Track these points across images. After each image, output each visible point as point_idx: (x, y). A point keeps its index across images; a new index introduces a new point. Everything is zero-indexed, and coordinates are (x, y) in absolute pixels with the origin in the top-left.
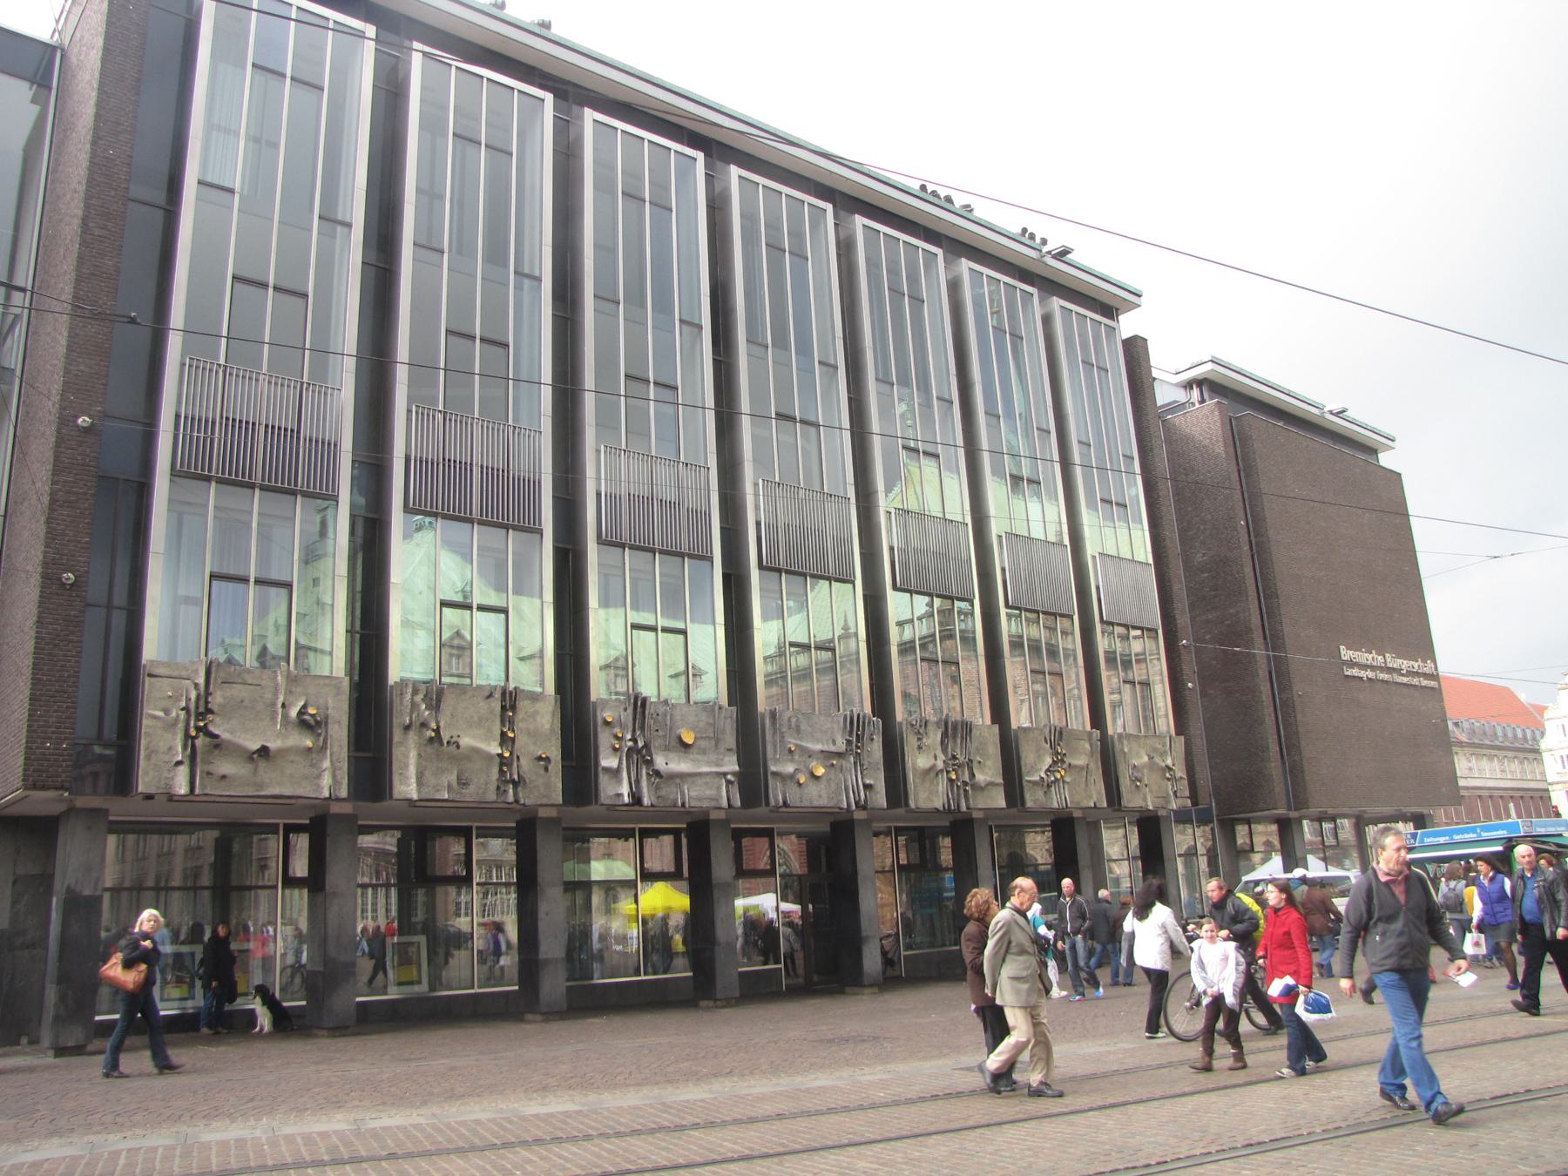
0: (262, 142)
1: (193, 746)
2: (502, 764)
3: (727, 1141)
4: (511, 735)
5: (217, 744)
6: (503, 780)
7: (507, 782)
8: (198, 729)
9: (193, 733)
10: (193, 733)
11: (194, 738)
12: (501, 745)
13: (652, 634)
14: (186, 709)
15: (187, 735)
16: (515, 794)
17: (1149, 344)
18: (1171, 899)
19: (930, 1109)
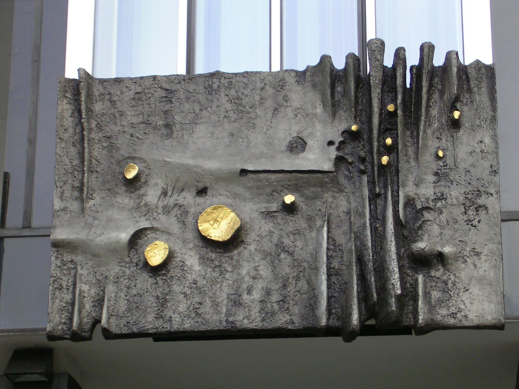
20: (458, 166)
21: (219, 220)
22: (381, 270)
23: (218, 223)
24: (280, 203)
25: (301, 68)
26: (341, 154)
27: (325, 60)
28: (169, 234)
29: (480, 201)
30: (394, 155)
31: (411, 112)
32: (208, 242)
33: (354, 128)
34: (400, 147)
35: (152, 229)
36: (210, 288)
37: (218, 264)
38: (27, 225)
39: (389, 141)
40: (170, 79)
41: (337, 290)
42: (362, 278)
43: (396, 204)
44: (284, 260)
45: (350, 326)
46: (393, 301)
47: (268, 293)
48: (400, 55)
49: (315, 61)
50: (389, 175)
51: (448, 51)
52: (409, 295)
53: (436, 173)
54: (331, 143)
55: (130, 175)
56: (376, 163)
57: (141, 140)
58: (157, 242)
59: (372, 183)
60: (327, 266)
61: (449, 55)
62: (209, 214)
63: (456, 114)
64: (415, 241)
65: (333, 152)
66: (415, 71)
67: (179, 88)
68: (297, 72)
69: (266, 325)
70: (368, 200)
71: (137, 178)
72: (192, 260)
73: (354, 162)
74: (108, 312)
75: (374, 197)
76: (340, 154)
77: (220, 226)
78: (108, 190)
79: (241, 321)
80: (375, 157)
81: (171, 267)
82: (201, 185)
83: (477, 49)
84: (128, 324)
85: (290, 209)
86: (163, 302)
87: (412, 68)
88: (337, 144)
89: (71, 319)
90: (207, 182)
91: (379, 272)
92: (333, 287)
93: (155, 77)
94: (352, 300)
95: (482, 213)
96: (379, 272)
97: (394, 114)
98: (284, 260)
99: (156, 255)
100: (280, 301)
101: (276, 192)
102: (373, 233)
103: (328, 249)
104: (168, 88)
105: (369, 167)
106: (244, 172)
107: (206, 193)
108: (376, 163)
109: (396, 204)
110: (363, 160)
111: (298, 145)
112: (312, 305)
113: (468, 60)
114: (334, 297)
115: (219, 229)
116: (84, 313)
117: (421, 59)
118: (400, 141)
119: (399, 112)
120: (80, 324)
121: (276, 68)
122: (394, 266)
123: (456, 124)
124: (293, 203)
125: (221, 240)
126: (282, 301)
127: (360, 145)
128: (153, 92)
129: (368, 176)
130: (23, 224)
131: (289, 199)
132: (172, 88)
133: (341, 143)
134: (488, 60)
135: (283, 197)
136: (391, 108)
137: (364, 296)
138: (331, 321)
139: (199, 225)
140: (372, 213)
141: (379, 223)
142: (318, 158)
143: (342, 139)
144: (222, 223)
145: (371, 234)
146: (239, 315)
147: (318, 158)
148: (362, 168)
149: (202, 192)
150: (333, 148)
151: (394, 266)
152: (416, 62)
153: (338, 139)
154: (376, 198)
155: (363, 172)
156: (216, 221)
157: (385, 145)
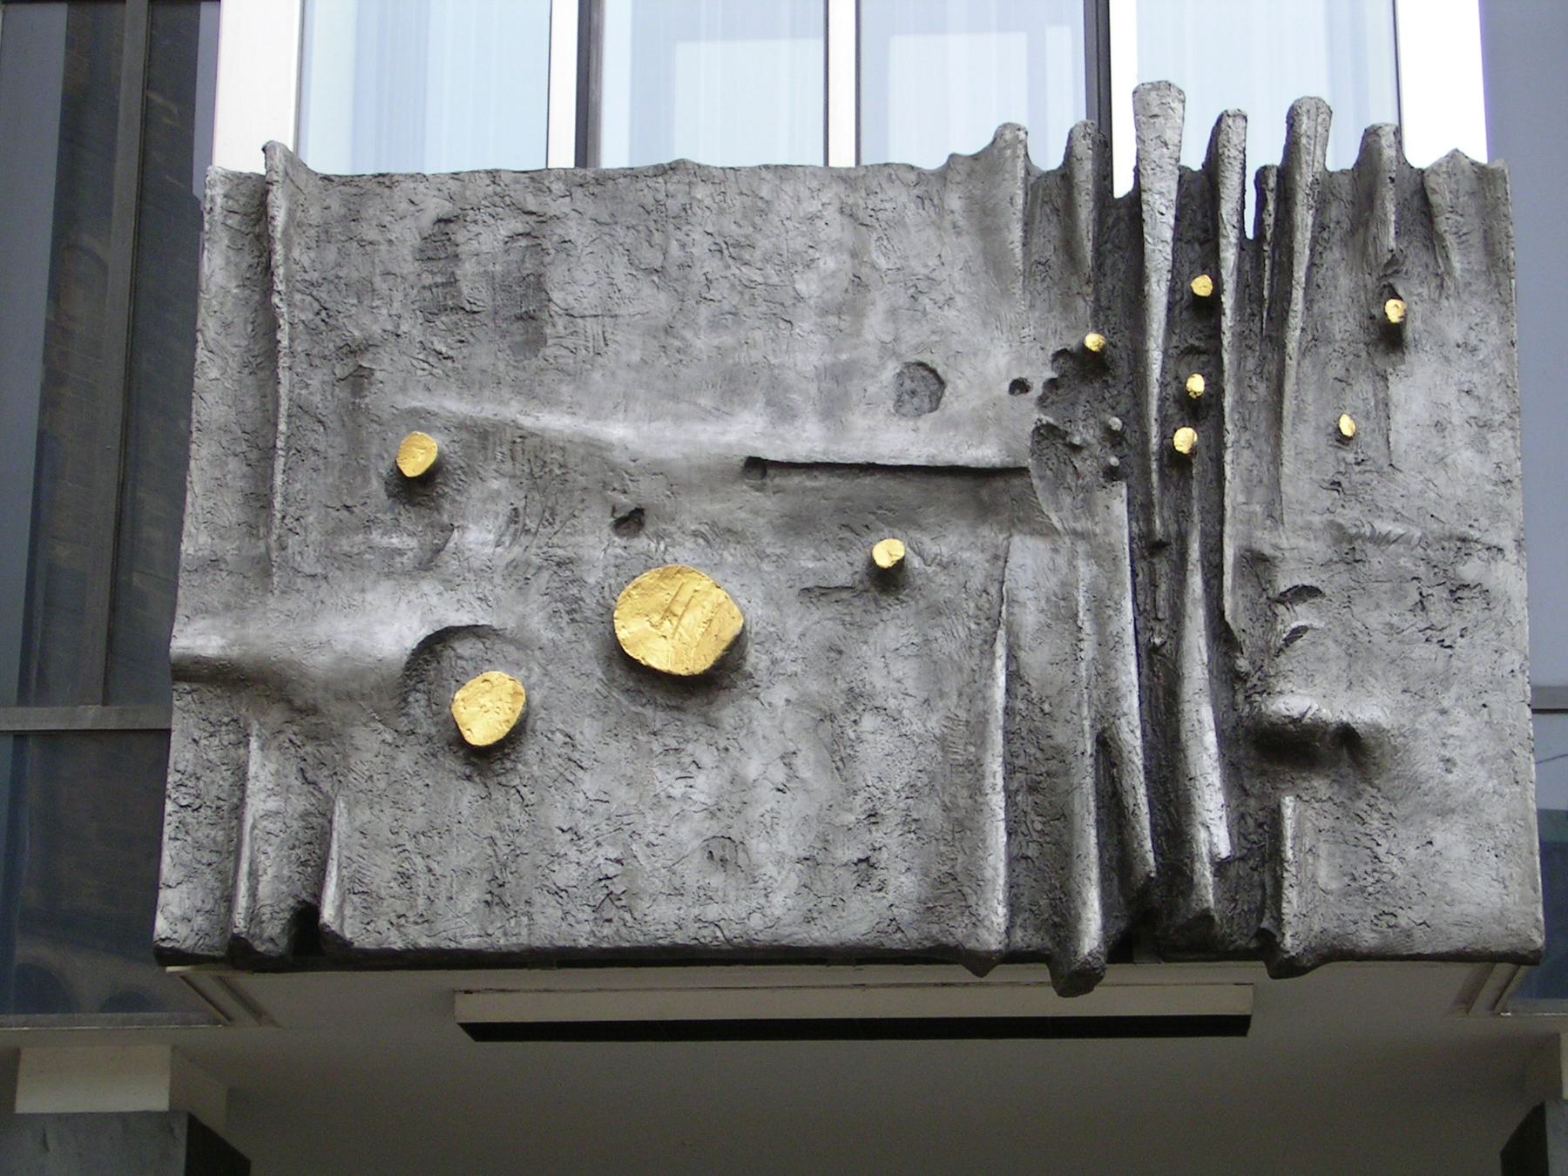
20: (1398, 465)
21: (678, 610)
23: (675, 621)
24: (860, 566)
25: (932, 161)
26: (1051, 420)
27: (1007, 142)
28: (522, 644)
29: (1469, 570)
30: (1208, 424)
31: (1261, 299)
33: (1093, 341)
34: (1228, 401)
35: (473, 631)
37: (674, 744)
39: (1196, 384)
40: (537, 179)
41: (1035, 836)
43: (1214, 573)
44: (870, 737)
45: (1076, 953)
46: (1205, 874)
49: (973, 142)
51: (1367, 125)
52: (1261, 846)
53: (1334, 483)
54: (1019, 386)
55: (415, 463)
57: (449, 363)
58: (494, 675)
59: (1141, 509)
60: (1006, 764)
61: (1371, 137)
62: (647, 592)
63: (1393, 311)
64: (1267, 691)
65: (1027, 414)
66: (1272, 182)
67: (567, 210)
68: (920, 173)
69: (817, 934)
70: (1128, 561)
71: (429, 478)
73: (1089, 445)
74: (339, 885)
75: (1148, 547)
76: (1048, 419)
77: (680, 629)
78: (347, 507)
79: (741, 922)
80: (1154, 430)
81: (530, 751)
82: (627, 502)
83: (1445, 122)
84: (403, 921)
85: (889, 581)
87: (1262, 174)
88: (1037, 389)
89: (229, 899)
90: (646, 491)
91: (1164, 784)
92: (1023, 828)
93: (493, 175)
94: (1079, 867)
95: (1473, 610)
96: (1164, 784)
97: (1209, 308)
98: (870, 737)
99: (484, 711)
100: (860, 861)
101: (858, 524)
102: (1145, 671)
103: (1009, 711)
104: (533, 209)
105: (1134, 461)
106: (757, 466)
107: (641, 525)
109: (1214, 573)
110: (1114, 439)
112: (952, 887)
113: (1422, 153)
114: (1027, 858)
115: (671, 637)
116: (264, 889)
117: (1292, 146)
118: (1229, 389)
119: (1228, 301)
120: (253, 916)
121: (842, 157)
123: (1391, 339)
124: (900, 565)
125: (684, 673)
126: (867, 860)
127: (1107, 395)
128: (486, 218)
129: (1129, 487)
131: (886, 552)
132: (546, 209)
133: (1052, 384)
134: (1478, 152)
135: (871, 545)
136: (1202, 286)
137: (1118, 860)
138: (1018, 934)
139: (618, 624)
140: (1141, 598)
141: (1160, 634)
143: (1054, 375)
144: (685, 621)
145: (1139, 666)
148: (1114, 461)
149: (631, 521)
150: (1028, 401)
152: (1275, 158)
153: (1040, 374)
154: (1152, 555)
155: (1112, 474)
156: (668, 612)
157: (1184, 394)
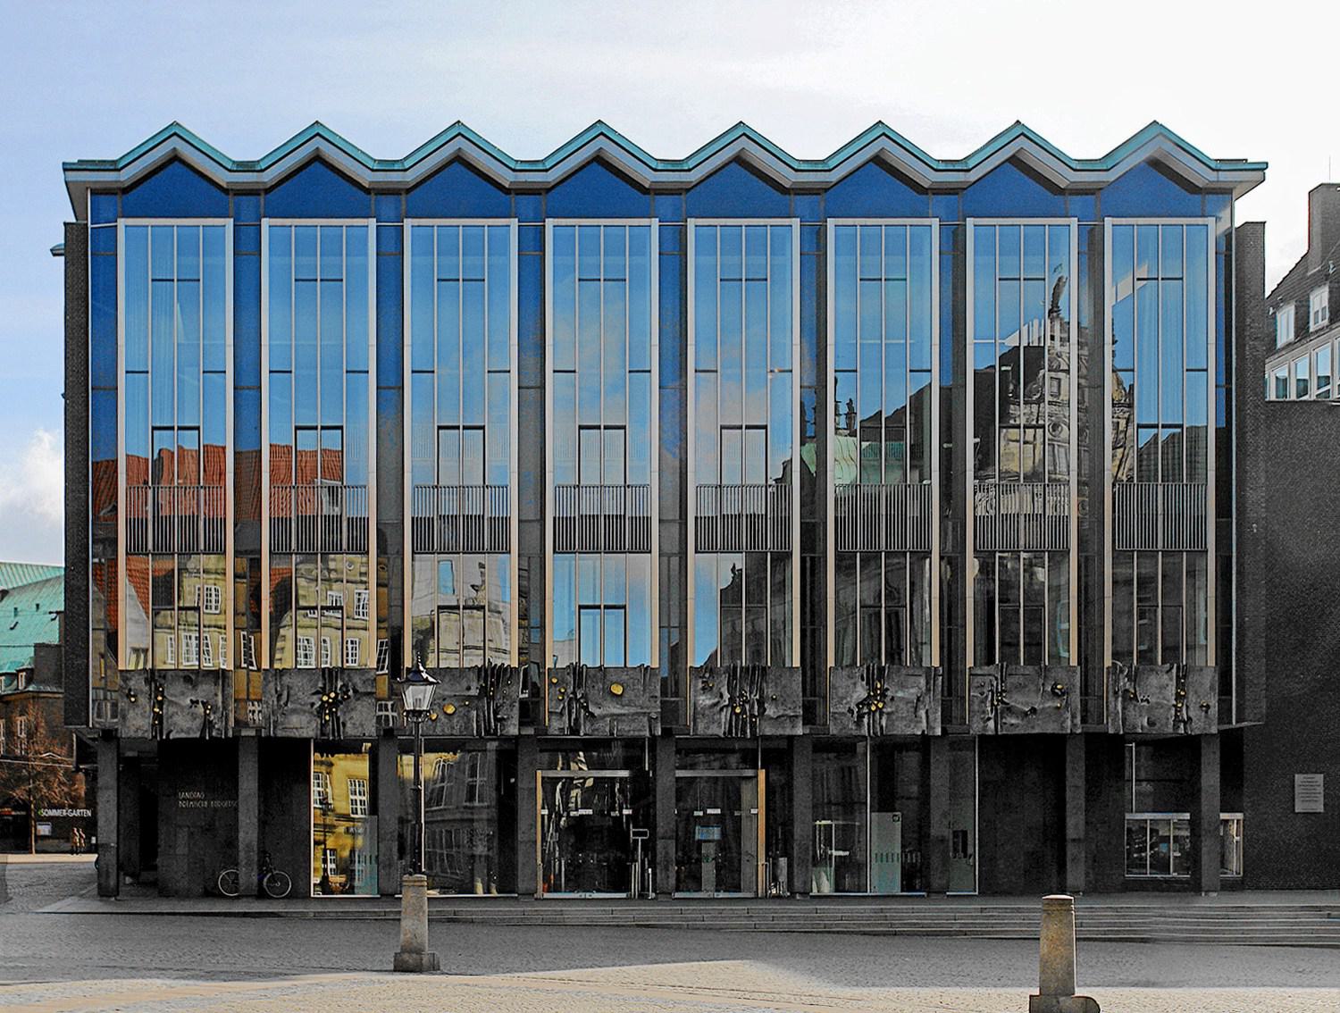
0: (1091, 482)
1: (996, 710)
2: (1176, 711)
3: (598, 582)
4: (1182, 693)
5: (1009, 710)
6: (1177, 720)
7: (1180, 721)
8: (998, 700)
9: (996, 703)
10: (996, 703)
11: (996, 706)
12: (1176, 700)
13: (597, 431)
14: (992, 691)
15: (992, 704)
16: (1185, 729)
17: (480, 125)
18: (1231, 186)
19: (666, 567)
22: (489, 722)
32: (445, 713)
36: (1255, 1002)
38: (238, 582)
42: (485, 724)
47: (461, 726)
48: (496, 665)
50: (493, 698)
56: (1120, 699)
72: (442, 717)
86: (435, 728)
106: (455, 696)
108: (1120, 699)
111: (469, 688)
122: (492, 721)
130: (71, 182)
142: (474, 692)
146: (1120, 979)
147: (474, 692)
151: (492, 721)
